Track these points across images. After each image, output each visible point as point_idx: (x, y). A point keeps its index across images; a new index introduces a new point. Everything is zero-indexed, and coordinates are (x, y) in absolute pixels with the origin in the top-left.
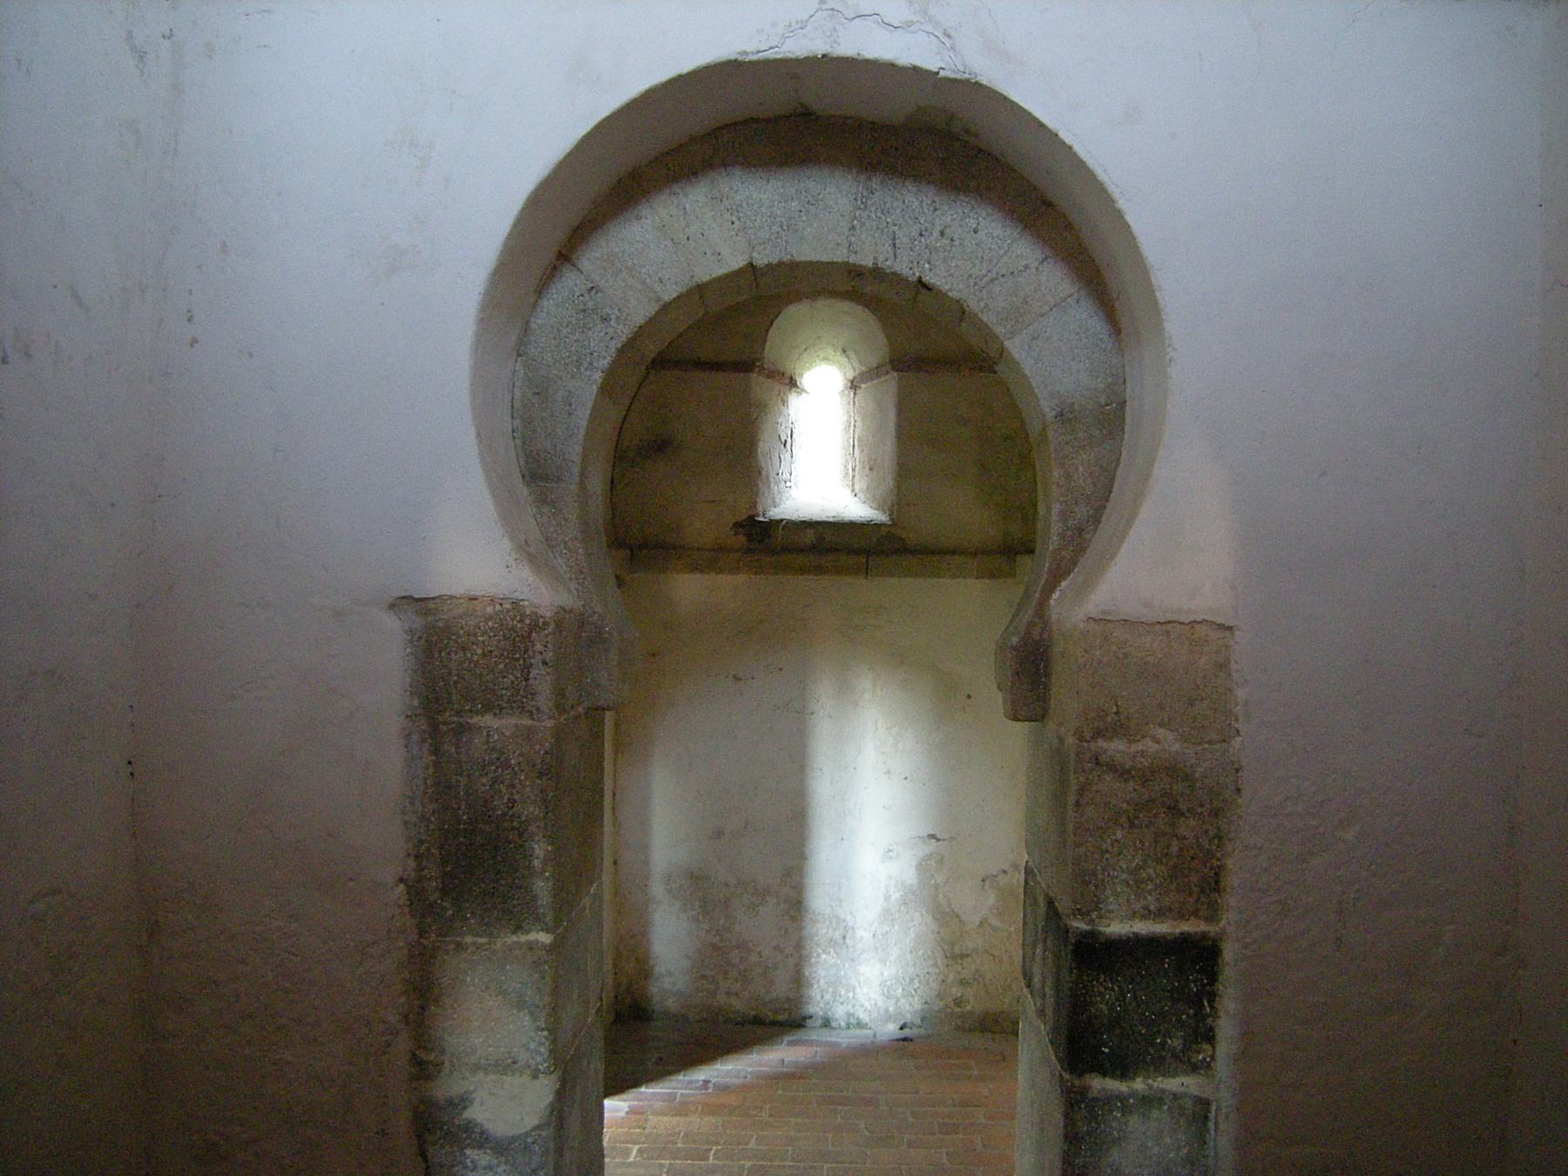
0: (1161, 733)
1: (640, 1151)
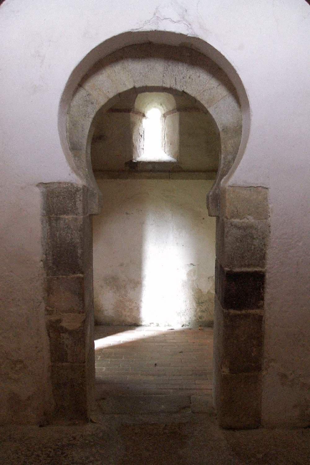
0: (249, 217)
1: (101, 357)
